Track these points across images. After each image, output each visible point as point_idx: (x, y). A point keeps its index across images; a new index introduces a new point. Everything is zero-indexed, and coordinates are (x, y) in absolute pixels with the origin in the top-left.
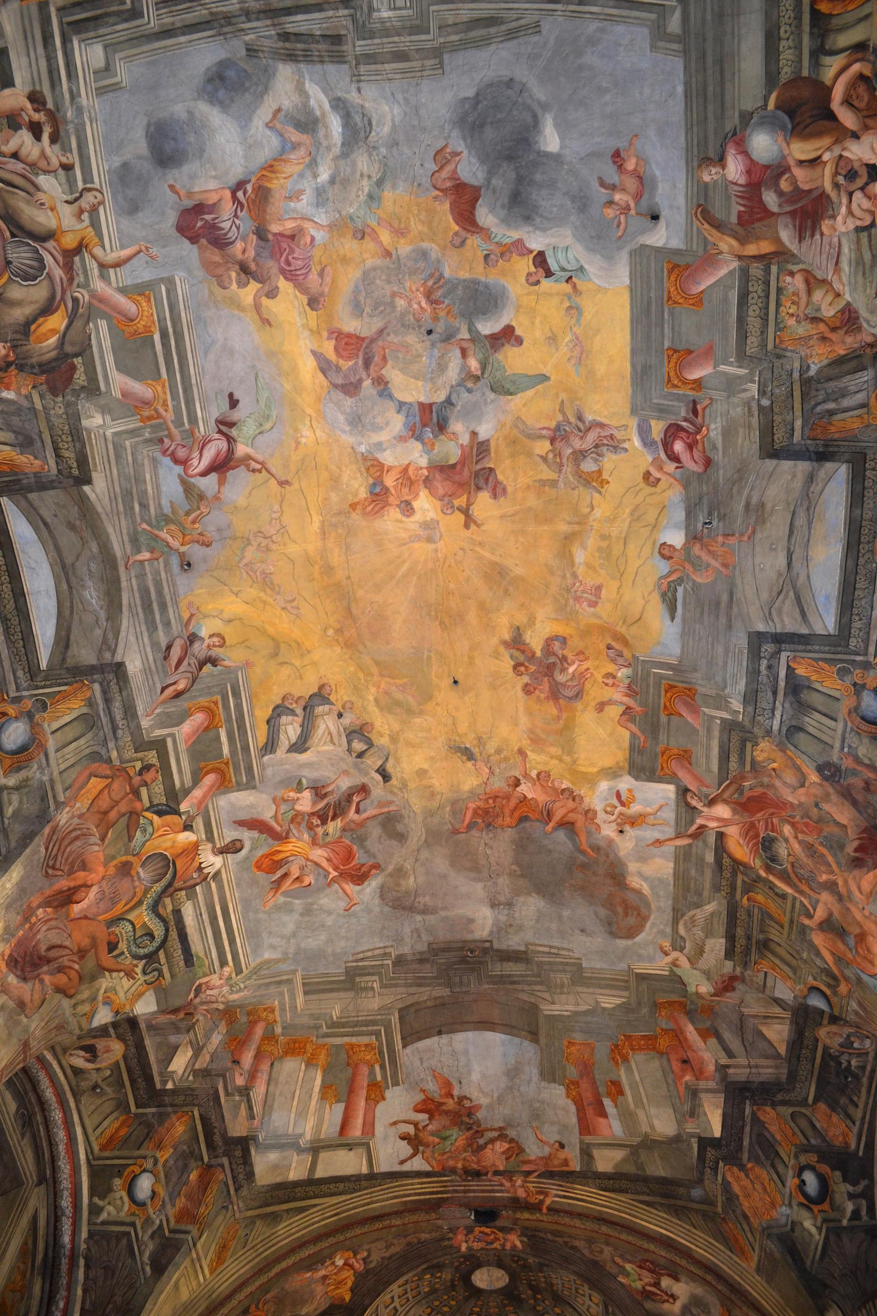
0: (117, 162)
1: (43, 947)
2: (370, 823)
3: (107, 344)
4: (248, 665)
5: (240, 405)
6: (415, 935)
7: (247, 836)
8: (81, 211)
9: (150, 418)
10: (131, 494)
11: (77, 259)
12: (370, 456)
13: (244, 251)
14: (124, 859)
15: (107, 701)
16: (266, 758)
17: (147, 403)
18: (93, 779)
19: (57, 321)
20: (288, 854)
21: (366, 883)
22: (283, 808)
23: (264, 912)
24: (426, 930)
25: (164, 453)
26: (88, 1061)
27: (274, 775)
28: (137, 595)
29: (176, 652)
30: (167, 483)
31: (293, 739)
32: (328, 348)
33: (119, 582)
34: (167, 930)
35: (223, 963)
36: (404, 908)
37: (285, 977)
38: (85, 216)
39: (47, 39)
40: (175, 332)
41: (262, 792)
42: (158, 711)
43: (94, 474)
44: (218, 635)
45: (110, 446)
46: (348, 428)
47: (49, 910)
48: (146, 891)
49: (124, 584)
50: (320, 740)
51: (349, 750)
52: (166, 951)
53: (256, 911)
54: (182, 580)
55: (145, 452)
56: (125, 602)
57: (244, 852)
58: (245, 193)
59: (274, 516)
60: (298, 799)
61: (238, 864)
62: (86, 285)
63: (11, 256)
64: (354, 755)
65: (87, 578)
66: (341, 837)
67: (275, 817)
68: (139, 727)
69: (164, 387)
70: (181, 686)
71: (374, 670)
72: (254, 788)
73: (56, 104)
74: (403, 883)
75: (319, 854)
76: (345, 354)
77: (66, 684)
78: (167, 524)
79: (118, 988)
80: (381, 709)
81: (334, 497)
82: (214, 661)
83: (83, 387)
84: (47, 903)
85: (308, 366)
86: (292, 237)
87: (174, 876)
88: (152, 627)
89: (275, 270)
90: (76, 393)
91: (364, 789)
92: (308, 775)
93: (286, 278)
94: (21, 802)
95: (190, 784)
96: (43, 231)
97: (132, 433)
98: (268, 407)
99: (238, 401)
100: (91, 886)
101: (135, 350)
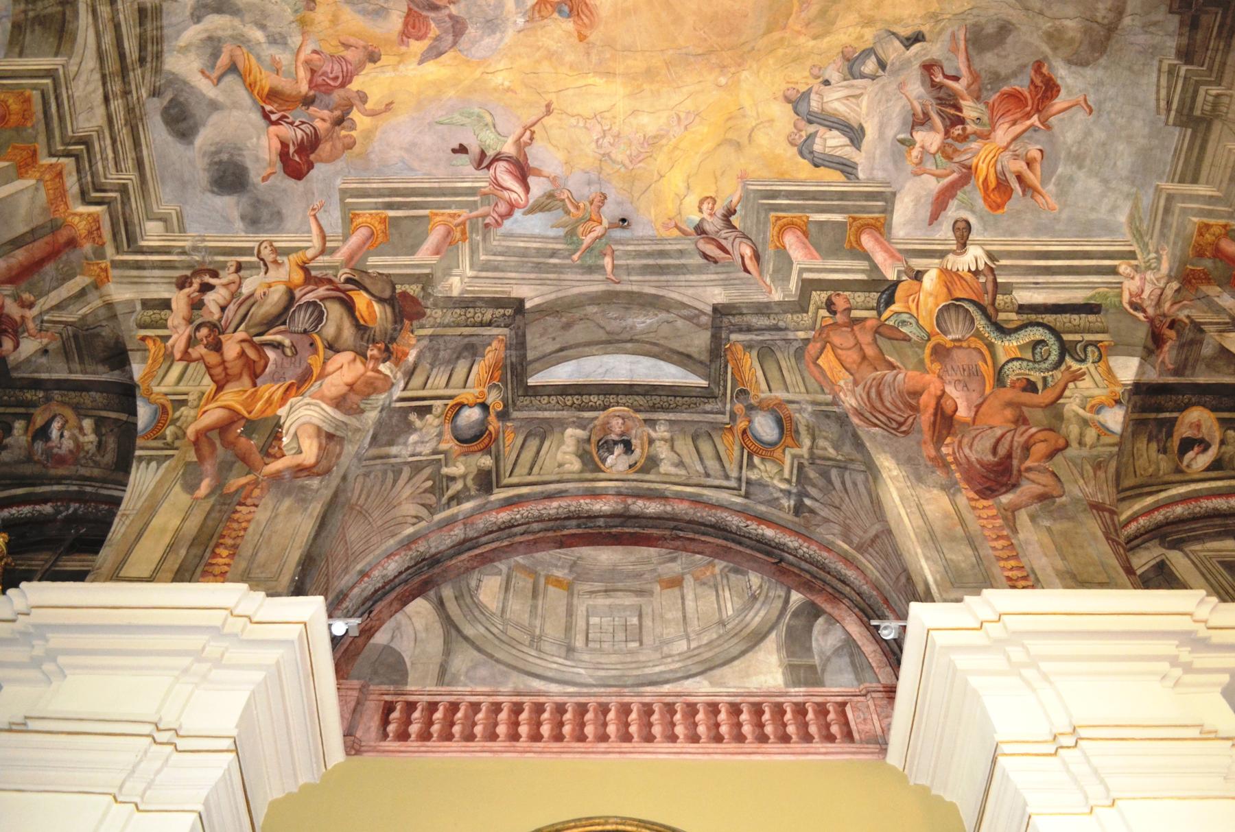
0: (239, 224)
1: (990, 458)
2: (977, 66)
3: (389, 260)
4: (743, 178)
5: (465, 143)
6: (1152, 29)
7: (953, 212)
8: (275, 262)
9: (463, 233)
10: (538, 262)
11: (313, 273)
12: (530, 13)
13: (323, 120)
14: (927, 351)
15: (749, 329)
16: (861, 175)
17: (449, 233)
18: (820, 362)
19: (361, 300)
20: (992, 171)
21: (1059, 82)
22: (929, 165)
23: (1061, 211)
24: (1148, 13)
25: (499, 224)
26: (1205, 450)
27: (885, 170)
28: (648, 278)
29: (712, 250)
30: (530, 227)
31: (845, 140)
32: (417, 47)
33: (633, 293)
34: (1039, 324)
35: (1113, 271)
36: (1108, 38)
37: (1162, 203)
38: (280, 259)
39: (139, 266)
40: (389, 196)
41: (902, 187)
42: (768, 280)
43: (513, 295)
44: (701, 202)
45: (484, 274)
46: (498, 35)
47: (948, 440)
48: (978, 335)
49: (635, 288)
50: (853, 110)
51: (873, 77)
52: (1067, 331)
53: (1056, 220)
54: (639, 230)
55: (495, 243)
56: (653, 291)
57: (972, 220)
58: (273, 113)
59: (581, 124)
60: (923, 147)
61: (985, 230)
62: (336, 268)
63: (301, 329)
64: (880, 72)
65: (624, 324)
66: (987, 103)
67: (938, 177)
68: (779, 303)
69: (436, 215)
70: (748, 252)
71: (776, 35)
72: (894, 194)
73: (189, 267)
74: (1071, 34)
75: (1003, 134)
76: (423, 30)
77: (726, 366)
78: (576, 235)
79: (1086, 393)
80: (827, 33)
81: (570, 57)
82: (730, 213)
83: (423, 288)
84: (938, 442)
85: (432, 70)
86: (313, 72)
87: (979, 303)
88: (682, 269)
89: (341, 92)
90: (427, 295)
91: (928, 67)
92: (895, 129)
93: (350, 82)
94: (825, 438)
95: (866, 263)
96: (285, 298)
97: (473, 251)
98: (470, 115)
99: (461, 145)
100: (944, 392)
101: (398, 234)
